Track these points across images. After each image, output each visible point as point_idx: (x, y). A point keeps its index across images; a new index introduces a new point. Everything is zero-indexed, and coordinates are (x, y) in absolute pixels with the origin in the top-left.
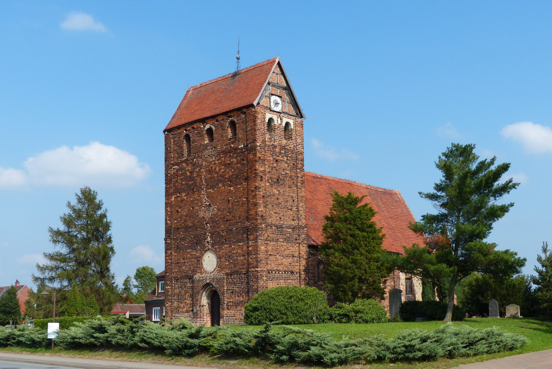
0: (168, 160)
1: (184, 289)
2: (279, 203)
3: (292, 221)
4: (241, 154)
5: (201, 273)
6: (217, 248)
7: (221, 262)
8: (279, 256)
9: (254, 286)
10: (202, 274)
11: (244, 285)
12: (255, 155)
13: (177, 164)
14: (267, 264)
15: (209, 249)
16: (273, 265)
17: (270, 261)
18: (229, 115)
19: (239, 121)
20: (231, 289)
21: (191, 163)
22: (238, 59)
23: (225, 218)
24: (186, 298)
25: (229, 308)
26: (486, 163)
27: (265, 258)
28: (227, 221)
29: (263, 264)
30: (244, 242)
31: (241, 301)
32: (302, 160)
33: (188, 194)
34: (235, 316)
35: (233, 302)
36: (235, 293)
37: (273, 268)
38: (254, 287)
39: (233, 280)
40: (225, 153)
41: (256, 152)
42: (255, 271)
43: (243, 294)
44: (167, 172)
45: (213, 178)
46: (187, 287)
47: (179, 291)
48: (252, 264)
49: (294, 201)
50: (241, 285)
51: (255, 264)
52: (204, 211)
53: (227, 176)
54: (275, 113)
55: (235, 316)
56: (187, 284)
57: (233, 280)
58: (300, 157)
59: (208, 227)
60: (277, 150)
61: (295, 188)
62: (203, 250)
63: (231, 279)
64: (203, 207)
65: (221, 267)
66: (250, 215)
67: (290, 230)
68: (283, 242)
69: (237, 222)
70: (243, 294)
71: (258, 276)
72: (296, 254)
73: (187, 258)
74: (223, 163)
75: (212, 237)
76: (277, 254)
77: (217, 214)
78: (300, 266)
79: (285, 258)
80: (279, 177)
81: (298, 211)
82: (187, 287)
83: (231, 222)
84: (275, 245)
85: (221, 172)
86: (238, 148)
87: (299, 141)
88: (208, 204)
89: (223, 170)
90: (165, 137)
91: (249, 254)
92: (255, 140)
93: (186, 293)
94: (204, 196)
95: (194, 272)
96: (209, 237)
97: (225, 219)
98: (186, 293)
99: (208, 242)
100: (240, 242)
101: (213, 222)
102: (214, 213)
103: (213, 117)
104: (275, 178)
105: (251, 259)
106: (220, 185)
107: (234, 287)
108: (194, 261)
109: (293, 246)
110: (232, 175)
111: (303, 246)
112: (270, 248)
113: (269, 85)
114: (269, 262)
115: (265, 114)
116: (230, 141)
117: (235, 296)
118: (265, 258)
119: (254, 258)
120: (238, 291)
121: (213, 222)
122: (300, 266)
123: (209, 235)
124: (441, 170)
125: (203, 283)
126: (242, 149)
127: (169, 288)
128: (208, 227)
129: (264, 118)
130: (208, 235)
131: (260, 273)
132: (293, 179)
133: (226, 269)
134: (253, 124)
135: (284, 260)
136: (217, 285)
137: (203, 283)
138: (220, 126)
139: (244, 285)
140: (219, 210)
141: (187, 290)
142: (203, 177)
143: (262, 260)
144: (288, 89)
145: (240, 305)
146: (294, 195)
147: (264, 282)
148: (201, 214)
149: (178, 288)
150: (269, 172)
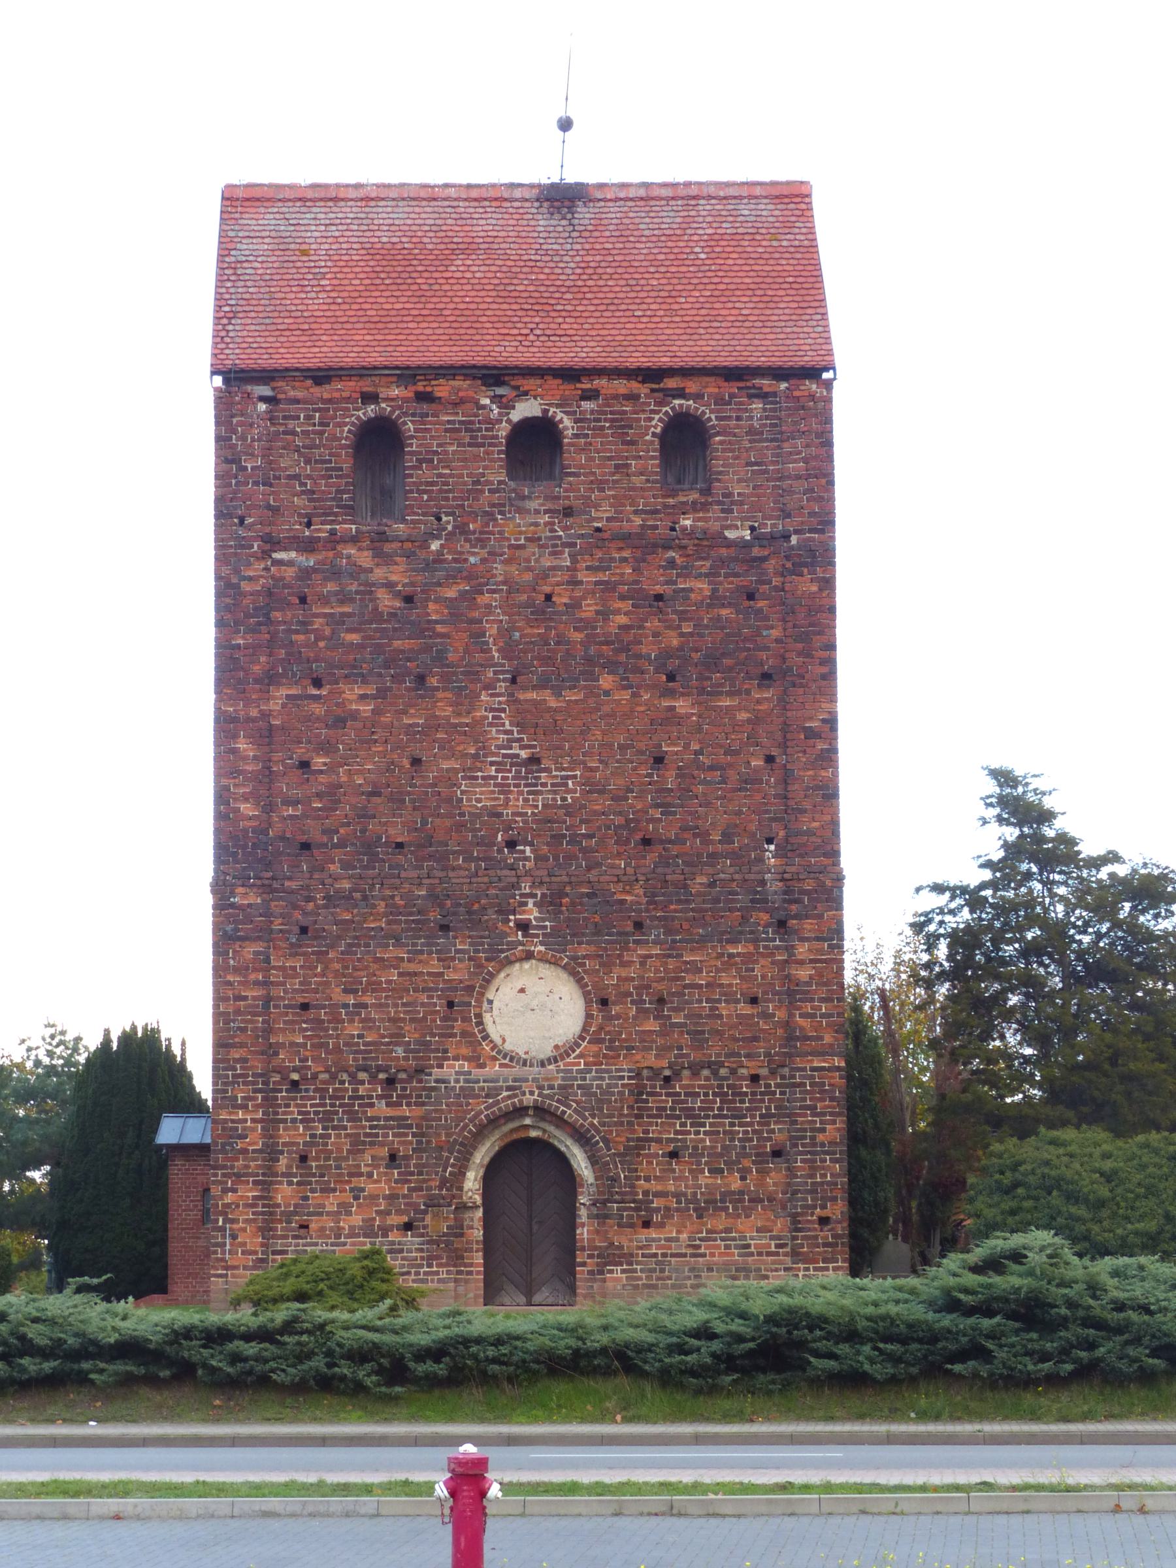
1: (345, 1128)
5: (477, 1061)
9: (823, 1130)
13: (308, 546)
18: (671, 383)
20: (669, 1140)
26: (115, 1046)
31: (733, 1193)
33: (382, 693)
34: (704, 1255)
35: (678, 1195)
38: (820, 1137)
42: (829, 1069)
44: (237, 571)
47: (313, 1136)
55: (704, 1255)
56: (372, 1105)
57: (683, 1102)
59: (527, 859)
63: (668, 1095)
64: (492, 764)
65: (612, 1041)
66: (800, 833)
69: (713, 856)
70: (746, 1163)
73: (374, 987)
86: (718, 540)
88: (524, 754)
89: (622, 620)
96: (531, 902)
99: (524, 926)
100: (734, 941)
103: (569, 374)
113: (570, 508)
116: (671, 501)
119: (823, 1016)
124: (93, 1042)
125: (498, 1102)
138: (612, 420)
140: (593, 788)
145: (726, 1209)
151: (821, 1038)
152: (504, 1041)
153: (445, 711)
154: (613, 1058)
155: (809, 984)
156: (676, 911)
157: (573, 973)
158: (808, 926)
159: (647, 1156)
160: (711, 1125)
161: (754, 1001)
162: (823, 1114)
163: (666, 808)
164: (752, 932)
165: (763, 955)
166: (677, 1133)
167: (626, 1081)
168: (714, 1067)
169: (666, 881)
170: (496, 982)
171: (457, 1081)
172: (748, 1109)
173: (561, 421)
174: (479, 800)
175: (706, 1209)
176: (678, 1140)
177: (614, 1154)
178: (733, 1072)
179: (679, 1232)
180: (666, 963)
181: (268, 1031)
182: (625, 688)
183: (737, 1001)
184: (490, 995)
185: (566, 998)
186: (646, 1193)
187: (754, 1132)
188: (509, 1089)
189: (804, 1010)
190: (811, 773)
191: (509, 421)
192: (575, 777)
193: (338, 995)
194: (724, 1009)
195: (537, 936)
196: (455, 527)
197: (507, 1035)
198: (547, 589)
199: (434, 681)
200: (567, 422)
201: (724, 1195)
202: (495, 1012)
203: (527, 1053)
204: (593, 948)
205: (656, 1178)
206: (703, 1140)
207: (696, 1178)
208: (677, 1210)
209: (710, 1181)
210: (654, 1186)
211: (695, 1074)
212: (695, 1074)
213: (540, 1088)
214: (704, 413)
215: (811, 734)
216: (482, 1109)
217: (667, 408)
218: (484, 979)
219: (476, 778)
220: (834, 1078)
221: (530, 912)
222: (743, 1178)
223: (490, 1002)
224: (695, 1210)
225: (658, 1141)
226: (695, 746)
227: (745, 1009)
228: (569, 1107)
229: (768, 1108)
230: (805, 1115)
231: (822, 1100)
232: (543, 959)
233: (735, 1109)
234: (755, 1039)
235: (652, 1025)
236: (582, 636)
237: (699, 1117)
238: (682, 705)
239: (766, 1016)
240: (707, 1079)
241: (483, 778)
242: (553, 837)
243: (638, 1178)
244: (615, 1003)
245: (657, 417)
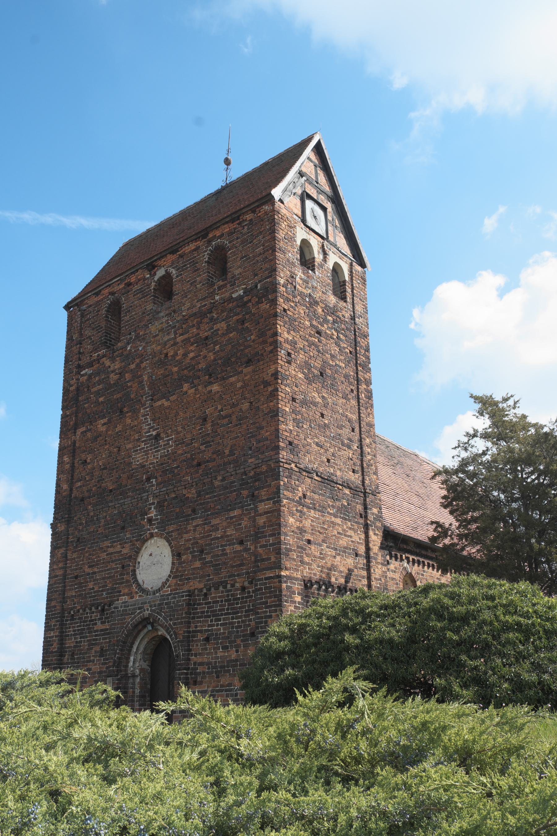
0: (71, 361)
3: (351, 473)
4: (238, 310)
6: (172, 532)
7: (180, 563)
8: (328, 547)
10: (132, 598)
11: (240, 617)
12: (274, 302)
13: (90, 365)
14: (302, 562)
15: (152, 536)
16: (314, 566)
17: (308, 555)
19: (234, 243)
21: (121, 355)
22: (227, 162)
23: (193, 459)
24: (92, 658)
25: (199, 679)
27: (298, 547)
28: (199, 465)
29: (294, 560)
30: (242, 507)
31: (233, 661)
32: (367, 350)
35: (208, 664)
36: (216, 639)
39: (212, 607)
40: (201, 315)
41: (276, 297)
43: (239, 641)
45: (168, 375)
46: (95, 631)
48: (263, 560)
50: (233, 618)
51: (273, 559)
52: (144, 452)
53: (202, 365)
57: (212, 607)
62: (137, 541)
63: (206, 604)
68: (336, 516)
71: (281, 591)
72: (362, 550)
74: (192, 340)
75: (160, 506)
76: (323, 541)
77: (174, 453)
78: (369, 578)
79: (339, 554)
81: (362, 454)
82: (95, 631)
83: (210, 465)
84: (318, 519)
85: (188, 360)
87: (359, 308)
88: (154, 433)
89: (191, 355)
90: (69, 317)
91: (258, 535)
92: (275, 270)
93: (91, 645)
94: (145, 419)
95: (115, 593)
97: (195, 463)
98: (91, 645)
99: (150, 520)
101: (164, 472)
102: (168, 451)
105: (261, 547)
106: (186, 386)
107: (213, 625)
108: (114, 569)
110: (215, 360)
111: (375, 534)
112: (307, 523)
114: (306, 559)
117: (214, 649)
118: (298, 547)
119: (271, 545)
120: (224, 633)
121: (164, 472)
122: (369, 578)
123: (153, 503)
125: (135, 617)
126: (240, 297)
127: (53, 637)
128: (153, 486)
130: (150, 504)
131: (286, 582)
133: (195, 578)
134: (270, 237)
135: (338, 558)
136: (171, 620)
137: (135, 617)
139: (240, 617)
140: (180, 442)
141: (94, 640)
142: (145, 378)
144: (336, 199)
147: (296, 607)
148: (138, 459)
149: (75, 635)
151: (270, 559)
152: (144, 583)
153: (128, 421)
154: (181, 585)
155: (264, 527)
156: (208, 498)
157: (168, 541)
158: (263, 493)
159: (196, 641)
160: (224, 619)
161: (241, 543)
162: (271, 606)
163: (207, 443)
164: (241, 503)
165: (245, 515)
166: (209, 626)
167: (184, 598)
168: (224, 584)
169: (204, 483)
170: (142, 551)
171: (121, 607)
172: (240, 608)
173: (172, 272)
174: (138, 461)
175: (220, 672)
176: (209, 630)
177: (178, 641)
178: (233, 585)
179: (208, 687)
180: (204, 528)
181: (64, 591)
182: (192, 388)
183: (234, 544)
184: (139, 560)
185: (167, 556)
186: (195, 664)
187: (243, 621)
188: (140, 608)
189: (262, 543)
190: (266, 405)
191: (154, 281)
192: (172, 439)
193: (88, 570)
194: (228, 549)
195: (154, 524)
196: (135, 336)
197: (144, 578)
198: (165, 351)
199: (125, 409)
200: (174, 272)
201: (228, 662)
202: (141, 568)
203: (152, 588)
204: (175, 526)
205: (200, 654)
206: (220, 629)
207: (216, 653)
208: (208, 673)
209: (222, 654)
210: (199, 659)
211: (217, 589)
212: (217, 589)
213: (151, 606)
214: (224, 242)
215: (267, 384)
216: (130, 621)
217: (210, 248)
218: (135, 551)
219: (137, 450)
220: (275, 582)
221: (152, 513)
222: (237, 651)
223: (139, 563)
224: (216, 672)
225: (200, 631)
226: (219, 407)
227: (238, 547)
228: (161, 615)
229: (249, 606)
230: (262, 608)
231: (270, 597)
232: (157, 535)
233: (234, 608)
234: (242, 565)
235: (198, 564)
236: (177, 368)
237: (218, 615)
238: (215, 388)
239: (247, 550)
240: (222, 592)
241: (140, 450)
242: (162, 472)
243: (192, 655)
244: (184, 554)
245: (206, 253)
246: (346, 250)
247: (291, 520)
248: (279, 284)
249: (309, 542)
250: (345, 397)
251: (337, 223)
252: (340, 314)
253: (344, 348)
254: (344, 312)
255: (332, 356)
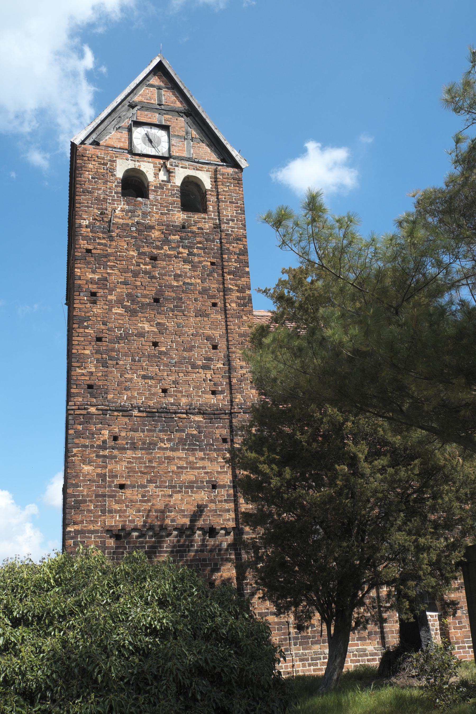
2: (161, 353)
27: (97, 496)
32: (244, 252)
37: (133, 521)
49: (215, 347)
54: (150, 160)
58: (235, 247)
60: (156, 234)
61: (220, 317)
67: (199, 418)
76: (149, 482)
79: (180, 492)
80: (160, 292)
104: (145, 296)
109: (211, 460)
115: (115, 161)
129: (112, 171)
132: (213, 297)
143: (85, 501)
146: (218, 333)
150: (125, 283)
246: (213, 158)
247: (86, 468)
248: (80, 226)
249: (122, 487)
250: (201, 314)
251: (194, 133)
252: (195, 229)
253: (200, 262)
254: (200, 225)
255: (177, 277)
